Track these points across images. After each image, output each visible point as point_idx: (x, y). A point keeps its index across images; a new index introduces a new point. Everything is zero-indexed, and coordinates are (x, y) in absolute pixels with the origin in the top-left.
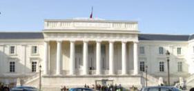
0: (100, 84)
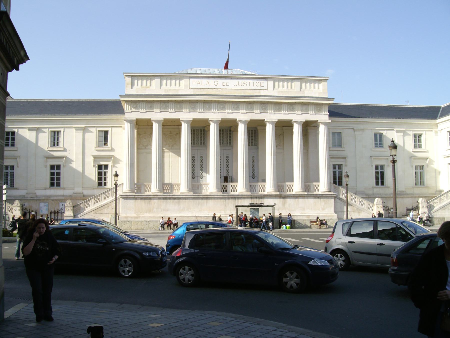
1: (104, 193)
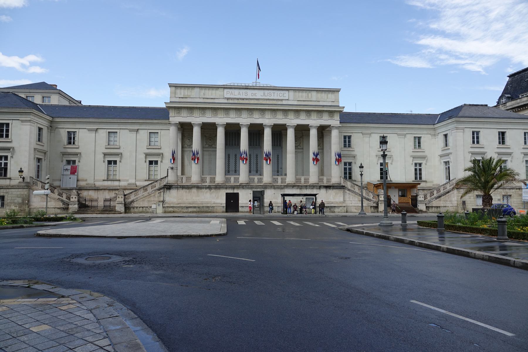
1: (151, 184)
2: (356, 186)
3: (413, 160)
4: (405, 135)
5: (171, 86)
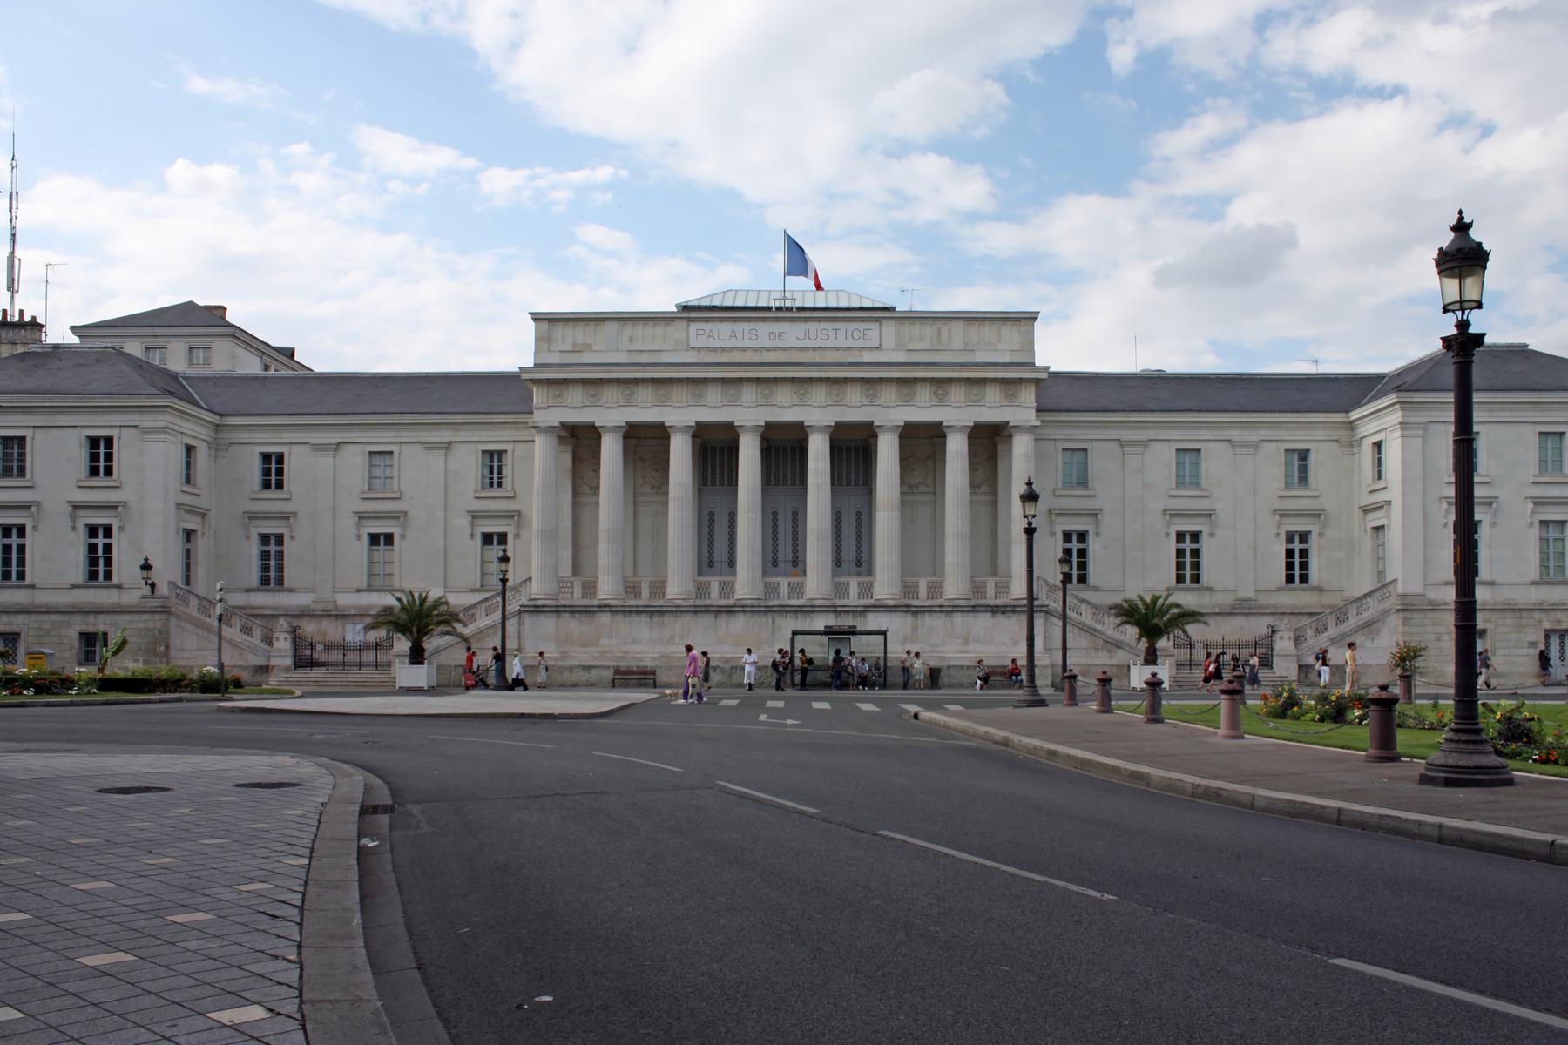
0: (818, 650)
1: (486, 600)
2: (1084, 607)
3: (1280, 524)
4: (1255, 445)
5: (537, 318)
